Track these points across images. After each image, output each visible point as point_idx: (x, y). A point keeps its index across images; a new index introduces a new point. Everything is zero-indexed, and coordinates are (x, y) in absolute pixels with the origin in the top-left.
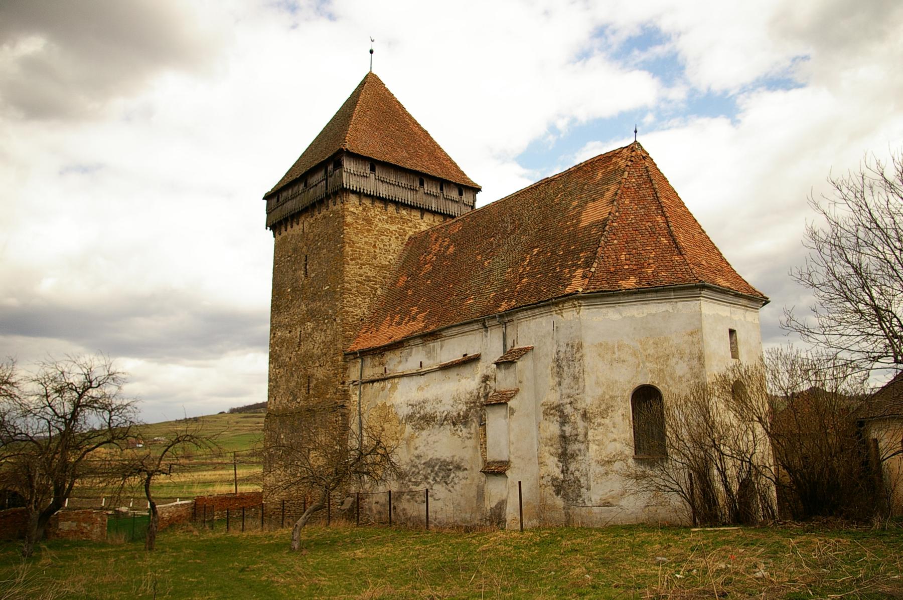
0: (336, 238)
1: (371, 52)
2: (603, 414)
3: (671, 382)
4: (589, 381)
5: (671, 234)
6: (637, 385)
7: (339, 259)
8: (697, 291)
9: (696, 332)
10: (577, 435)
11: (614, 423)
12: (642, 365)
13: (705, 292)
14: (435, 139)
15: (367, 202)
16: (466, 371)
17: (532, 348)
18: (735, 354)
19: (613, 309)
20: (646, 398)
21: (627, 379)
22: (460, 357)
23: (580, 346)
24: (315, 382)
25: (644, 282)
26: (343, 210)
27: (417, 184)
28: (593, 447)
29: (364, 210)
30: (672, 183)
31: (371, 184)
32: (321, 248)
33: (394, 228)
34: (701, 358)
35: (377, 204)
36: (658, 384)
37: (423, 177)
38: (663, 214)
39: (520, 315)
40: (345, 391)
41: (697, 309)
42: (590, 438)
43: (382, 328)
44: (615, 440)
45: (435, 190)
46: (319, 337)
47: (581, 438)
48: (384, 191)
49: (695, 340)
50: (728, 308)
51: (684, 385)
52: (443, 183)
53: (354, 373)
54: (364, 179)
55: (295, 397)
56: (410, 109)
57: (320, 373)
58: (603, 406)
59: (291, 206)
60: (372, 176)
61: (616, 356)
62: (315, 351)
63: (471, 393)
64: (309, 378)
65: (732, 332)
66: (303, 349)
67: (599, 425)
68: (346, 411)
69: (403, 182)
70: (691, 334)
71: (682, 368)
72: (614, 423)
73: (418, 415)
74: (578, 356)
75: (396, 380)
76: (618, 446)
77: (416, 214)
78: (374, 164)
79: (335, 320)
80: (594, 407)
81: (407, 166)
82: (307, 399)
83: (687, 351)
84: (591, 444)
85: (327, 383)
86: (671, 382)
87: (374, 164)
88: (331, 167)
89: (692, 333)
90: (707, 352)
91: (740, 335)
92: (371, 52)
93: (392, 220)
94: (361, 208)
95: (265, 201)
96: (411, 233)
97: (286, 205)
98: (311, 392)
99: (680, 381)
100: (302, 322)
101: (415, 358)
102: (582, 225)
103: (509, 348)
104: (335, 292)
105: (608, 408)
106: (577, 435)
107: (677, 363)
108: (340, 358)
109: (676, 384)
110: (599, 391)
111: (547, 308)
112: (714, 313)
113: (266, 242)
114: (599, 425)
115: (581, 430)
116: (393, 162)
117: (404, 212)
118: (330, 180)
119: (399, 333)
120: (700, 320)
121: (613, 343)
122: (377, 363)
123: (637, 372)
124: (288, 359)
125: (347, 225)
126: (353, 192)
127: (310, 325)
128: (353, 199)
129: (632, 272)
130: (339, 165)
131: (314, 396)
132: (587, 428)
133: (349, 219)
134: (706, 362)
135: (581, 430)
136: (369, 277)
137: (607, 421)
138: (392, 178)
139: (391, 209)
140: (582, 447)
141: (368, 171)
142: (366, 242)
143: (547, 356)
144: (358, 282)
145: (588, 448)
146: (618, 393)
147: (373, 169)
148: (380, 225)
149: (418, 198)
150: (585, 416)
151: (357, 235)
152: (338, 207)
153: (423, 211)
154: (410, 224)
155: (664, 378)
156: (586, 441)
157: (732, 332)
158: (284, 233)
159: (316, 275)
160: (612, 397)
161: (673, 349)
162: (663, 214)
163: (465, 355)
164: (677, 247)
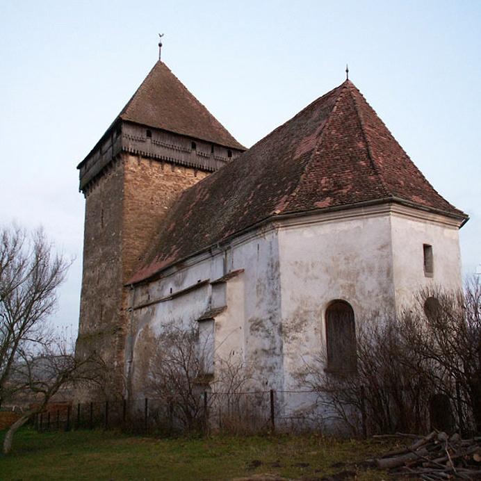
0: (118, 193)
1: (160, 45)
2: (297, 328)
3: (361, 297)
4: (285, 296)
5: (369, 157)
6: (329, 300)
7: (120, 212)
8: (386, 206)
9: (386, 245)
10: (275, 349)
11: (307, 337)
12: (333, 281)
13: (394, 207)
14: (211, 112)
15: (145, 162)
16: (199, 293)
17: (243, 270)
18: (428, 268)
19: (308, 229)
20: (339, 313)
21: (320, 294)
22: (195, 282)
23: (278, 265)
24: (105, 310)
25: (337, 202)
26: (124, 169)
27: (189, 147)
28: (287, 360)
29: (142, 169)
30: (379, 115)
31: (148, 146)
32: (110, 203)
33: (169, 184)
34: (389, 272)
35: (155, 164)
36: (349, 299)
37: (194, 142)
38: (365, 141)
39: (234, 242)
40: (122, 316)
41: (387, 222)
42: (285, 351)
43: (152, 264)
44: (307, 353)
45: (207, 152)
46: (109, 275)
47: (277, 351)
48: (159, 152)
49: (385, 254)
50: (422, 224)
51: (374, 299)
52: (214, 146)
53: (129, 301)
54: (141, 143)
55: (93, 322)
56: (190, 90)
57: (108, 303)
58: (298, 321)
59: (94, 170)
60: (149, 140)
61: (310, 274)
62: (107, 285)
63: (202, 313)
64: (102, 306)
65: (427, 248)
66: (100, 284)
67: (294, 338)
68: (123, 333)
69: (178, 145)
70: (383, 247)
71: (370, 283)
72: (307, 337)
73: (167, 335)
74: (276, 275)
75: (155, 306)
76: (309, 359)
77: (190, 172)
78: (150, 131)
79: (118, 260)
80: (289, 322)
81: (181, 133)
82: (100, 324)
83: (377, 265)
84: (285, 358)
85: (112, 310)
86: (361, 297)
87: (150, 131)
88: (115, 135)
89: (382, 247)
90: (397, 265)
91: (435, 251)
92: (160, 45)
93: (168, 177)
94: (140, 168)
95: (79, 170)
96: (185, 188)
97: (90, 170)
98: (103, 318)
99: (370, 296)
100: (100, 263)
101: (169, 287)
102: (295, 158)
103: (228, 272)
104: (118, 237)
105: (302, 322)
106: (275, 349)
107: (367, 278)
108: (120, 289)
109: (365, 298)
110: (294, 307)
111: (253, 233)
112: (405, 230)
113: (81, 199)
114: (294, 338)
115: (278, 345)
116: (166, 129)
117: (179, 171)
118: (115, 145)
119: (163, 264)
120: (389, 234)
121: (308, 258)
122: (144, 292)
123: (329, 288)
124: (91, 293)
125: (126, 182)
126: (133, 154)
127: (104, 265)
128: (133, 159)
129: (328, 194)
130: (120, 132)
131: (105, 322)
132: (282, 342)
133: (129, 177)
134: (394, 279)
135: (278, 345)
136: (146, 224)
137: (300, 335)
138: (168, 142)
139: (167, 168)
140: (278, 359)
141: (145, 137)
142: (144, 196)
143: (253, 276)
144: (136, 228)
145: (283, 361)
146: (312, 308)
147: (149, 135)
148: (157, 181)
149: (193, 157)
150: (281, 330)
151: (136, 189)
152: (121, 167)
153: (197, 169)
154: (185, 181)
155: (354, 293)
156: (281, 355)
157: (427, 248)
158: (91, 194)
159: (108, 225)
160: (306, 312)
161: (364, 264)
162: (365, 141)
163: (199, 281)
164: (374, 168)
